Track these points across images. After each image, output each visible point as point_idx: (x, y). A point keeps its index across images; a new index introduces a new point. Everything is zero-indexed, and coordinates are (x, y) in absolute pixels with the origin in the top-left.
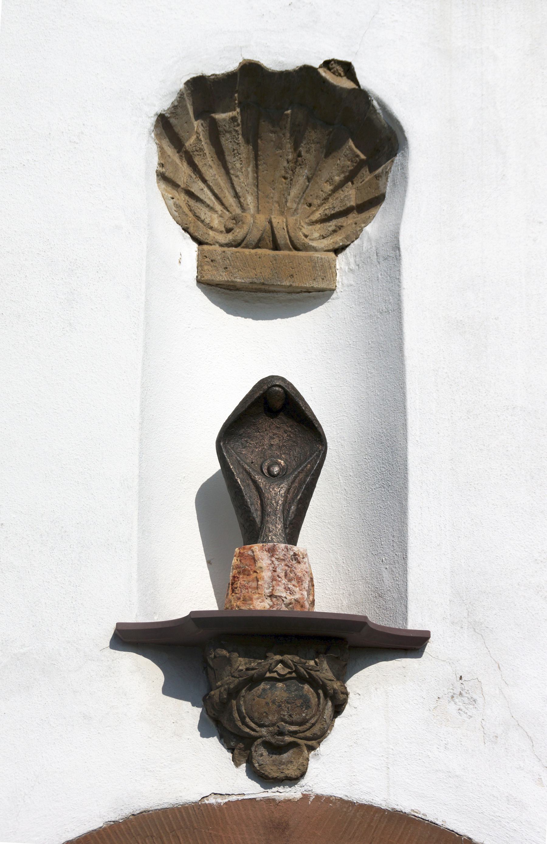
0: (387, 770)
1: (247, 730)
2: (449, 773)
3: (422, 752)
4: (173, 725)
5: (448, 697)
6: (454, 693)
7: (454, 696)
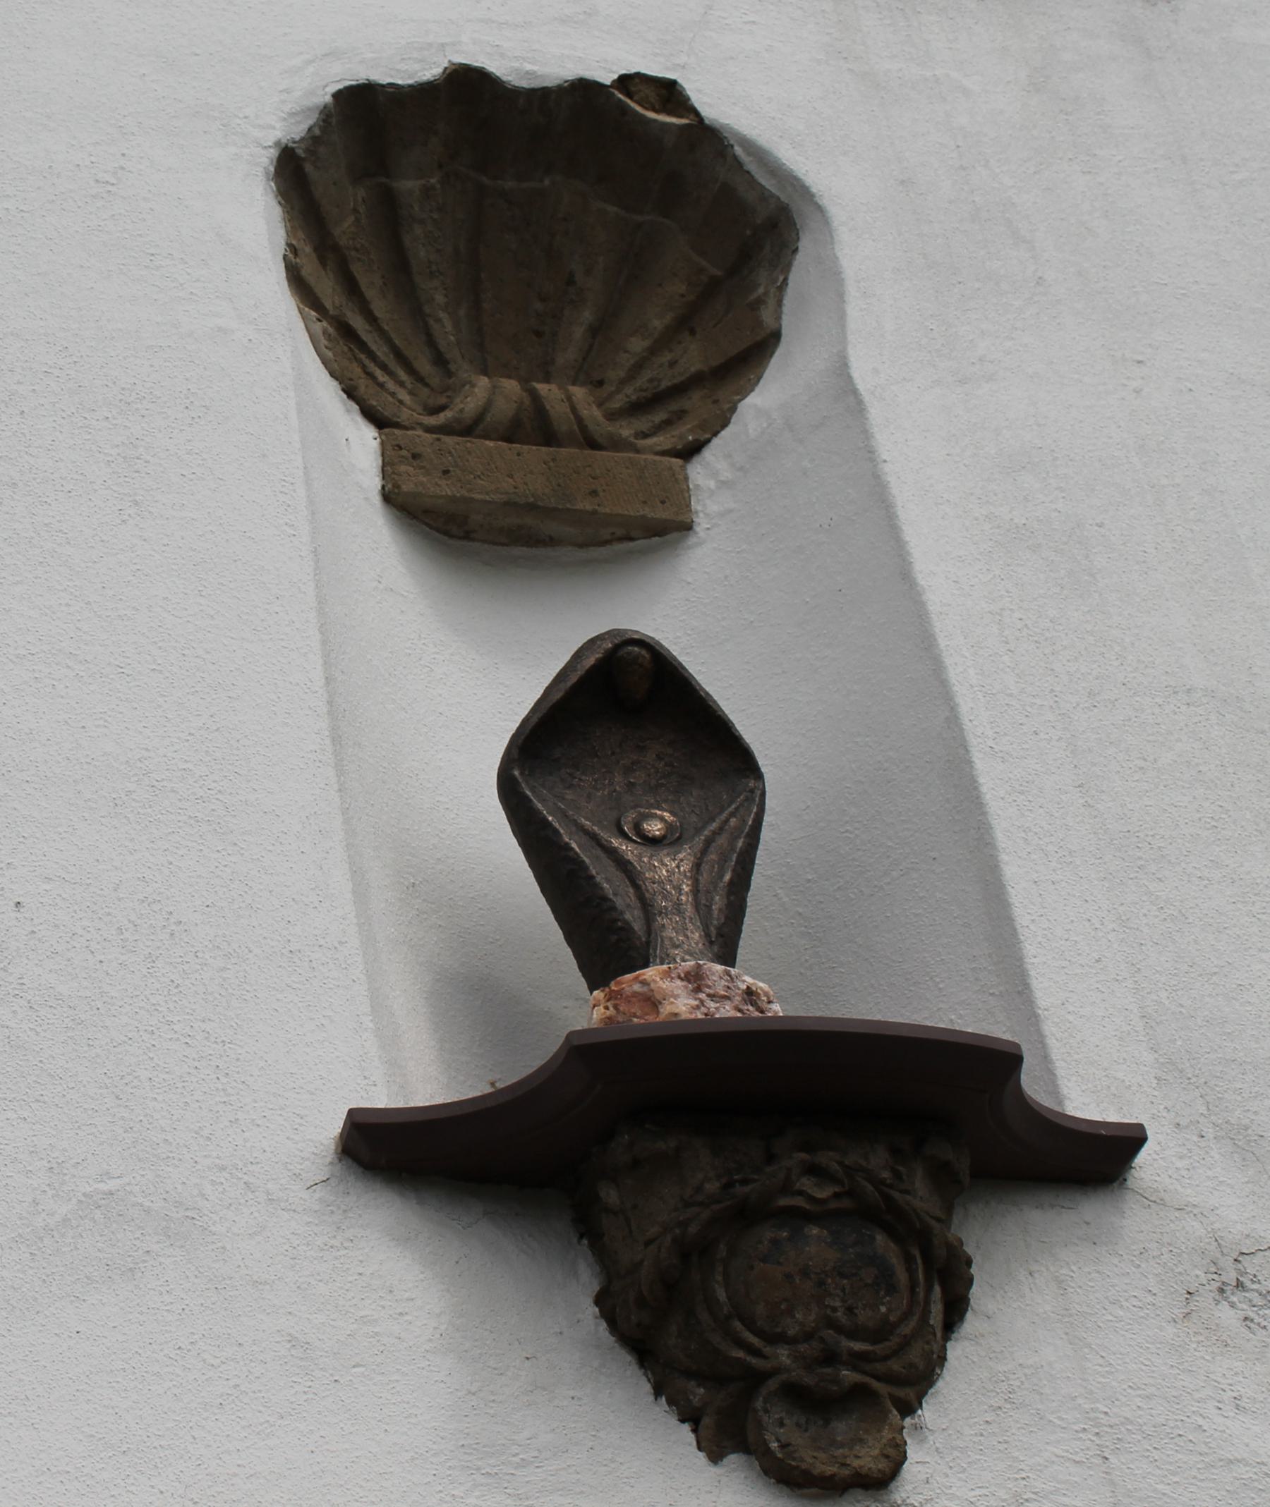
0: (1104, 1463)
1: (740, 1354)
2: (1262, 1466)
3: (1183, 1418)
4: (527, 1363)
5: (1210, 1291)
6: (1223, 1283)
7: (1225, 1288)
